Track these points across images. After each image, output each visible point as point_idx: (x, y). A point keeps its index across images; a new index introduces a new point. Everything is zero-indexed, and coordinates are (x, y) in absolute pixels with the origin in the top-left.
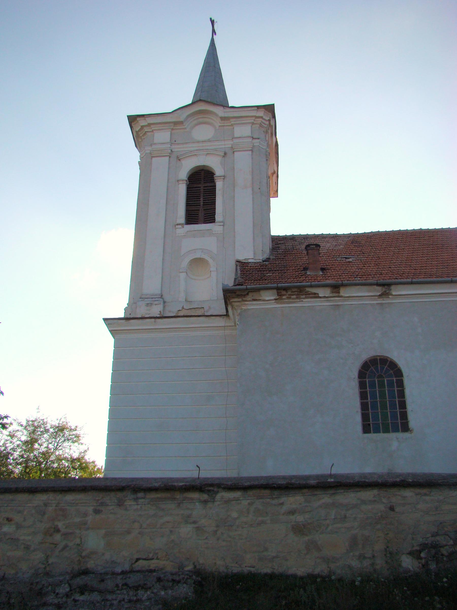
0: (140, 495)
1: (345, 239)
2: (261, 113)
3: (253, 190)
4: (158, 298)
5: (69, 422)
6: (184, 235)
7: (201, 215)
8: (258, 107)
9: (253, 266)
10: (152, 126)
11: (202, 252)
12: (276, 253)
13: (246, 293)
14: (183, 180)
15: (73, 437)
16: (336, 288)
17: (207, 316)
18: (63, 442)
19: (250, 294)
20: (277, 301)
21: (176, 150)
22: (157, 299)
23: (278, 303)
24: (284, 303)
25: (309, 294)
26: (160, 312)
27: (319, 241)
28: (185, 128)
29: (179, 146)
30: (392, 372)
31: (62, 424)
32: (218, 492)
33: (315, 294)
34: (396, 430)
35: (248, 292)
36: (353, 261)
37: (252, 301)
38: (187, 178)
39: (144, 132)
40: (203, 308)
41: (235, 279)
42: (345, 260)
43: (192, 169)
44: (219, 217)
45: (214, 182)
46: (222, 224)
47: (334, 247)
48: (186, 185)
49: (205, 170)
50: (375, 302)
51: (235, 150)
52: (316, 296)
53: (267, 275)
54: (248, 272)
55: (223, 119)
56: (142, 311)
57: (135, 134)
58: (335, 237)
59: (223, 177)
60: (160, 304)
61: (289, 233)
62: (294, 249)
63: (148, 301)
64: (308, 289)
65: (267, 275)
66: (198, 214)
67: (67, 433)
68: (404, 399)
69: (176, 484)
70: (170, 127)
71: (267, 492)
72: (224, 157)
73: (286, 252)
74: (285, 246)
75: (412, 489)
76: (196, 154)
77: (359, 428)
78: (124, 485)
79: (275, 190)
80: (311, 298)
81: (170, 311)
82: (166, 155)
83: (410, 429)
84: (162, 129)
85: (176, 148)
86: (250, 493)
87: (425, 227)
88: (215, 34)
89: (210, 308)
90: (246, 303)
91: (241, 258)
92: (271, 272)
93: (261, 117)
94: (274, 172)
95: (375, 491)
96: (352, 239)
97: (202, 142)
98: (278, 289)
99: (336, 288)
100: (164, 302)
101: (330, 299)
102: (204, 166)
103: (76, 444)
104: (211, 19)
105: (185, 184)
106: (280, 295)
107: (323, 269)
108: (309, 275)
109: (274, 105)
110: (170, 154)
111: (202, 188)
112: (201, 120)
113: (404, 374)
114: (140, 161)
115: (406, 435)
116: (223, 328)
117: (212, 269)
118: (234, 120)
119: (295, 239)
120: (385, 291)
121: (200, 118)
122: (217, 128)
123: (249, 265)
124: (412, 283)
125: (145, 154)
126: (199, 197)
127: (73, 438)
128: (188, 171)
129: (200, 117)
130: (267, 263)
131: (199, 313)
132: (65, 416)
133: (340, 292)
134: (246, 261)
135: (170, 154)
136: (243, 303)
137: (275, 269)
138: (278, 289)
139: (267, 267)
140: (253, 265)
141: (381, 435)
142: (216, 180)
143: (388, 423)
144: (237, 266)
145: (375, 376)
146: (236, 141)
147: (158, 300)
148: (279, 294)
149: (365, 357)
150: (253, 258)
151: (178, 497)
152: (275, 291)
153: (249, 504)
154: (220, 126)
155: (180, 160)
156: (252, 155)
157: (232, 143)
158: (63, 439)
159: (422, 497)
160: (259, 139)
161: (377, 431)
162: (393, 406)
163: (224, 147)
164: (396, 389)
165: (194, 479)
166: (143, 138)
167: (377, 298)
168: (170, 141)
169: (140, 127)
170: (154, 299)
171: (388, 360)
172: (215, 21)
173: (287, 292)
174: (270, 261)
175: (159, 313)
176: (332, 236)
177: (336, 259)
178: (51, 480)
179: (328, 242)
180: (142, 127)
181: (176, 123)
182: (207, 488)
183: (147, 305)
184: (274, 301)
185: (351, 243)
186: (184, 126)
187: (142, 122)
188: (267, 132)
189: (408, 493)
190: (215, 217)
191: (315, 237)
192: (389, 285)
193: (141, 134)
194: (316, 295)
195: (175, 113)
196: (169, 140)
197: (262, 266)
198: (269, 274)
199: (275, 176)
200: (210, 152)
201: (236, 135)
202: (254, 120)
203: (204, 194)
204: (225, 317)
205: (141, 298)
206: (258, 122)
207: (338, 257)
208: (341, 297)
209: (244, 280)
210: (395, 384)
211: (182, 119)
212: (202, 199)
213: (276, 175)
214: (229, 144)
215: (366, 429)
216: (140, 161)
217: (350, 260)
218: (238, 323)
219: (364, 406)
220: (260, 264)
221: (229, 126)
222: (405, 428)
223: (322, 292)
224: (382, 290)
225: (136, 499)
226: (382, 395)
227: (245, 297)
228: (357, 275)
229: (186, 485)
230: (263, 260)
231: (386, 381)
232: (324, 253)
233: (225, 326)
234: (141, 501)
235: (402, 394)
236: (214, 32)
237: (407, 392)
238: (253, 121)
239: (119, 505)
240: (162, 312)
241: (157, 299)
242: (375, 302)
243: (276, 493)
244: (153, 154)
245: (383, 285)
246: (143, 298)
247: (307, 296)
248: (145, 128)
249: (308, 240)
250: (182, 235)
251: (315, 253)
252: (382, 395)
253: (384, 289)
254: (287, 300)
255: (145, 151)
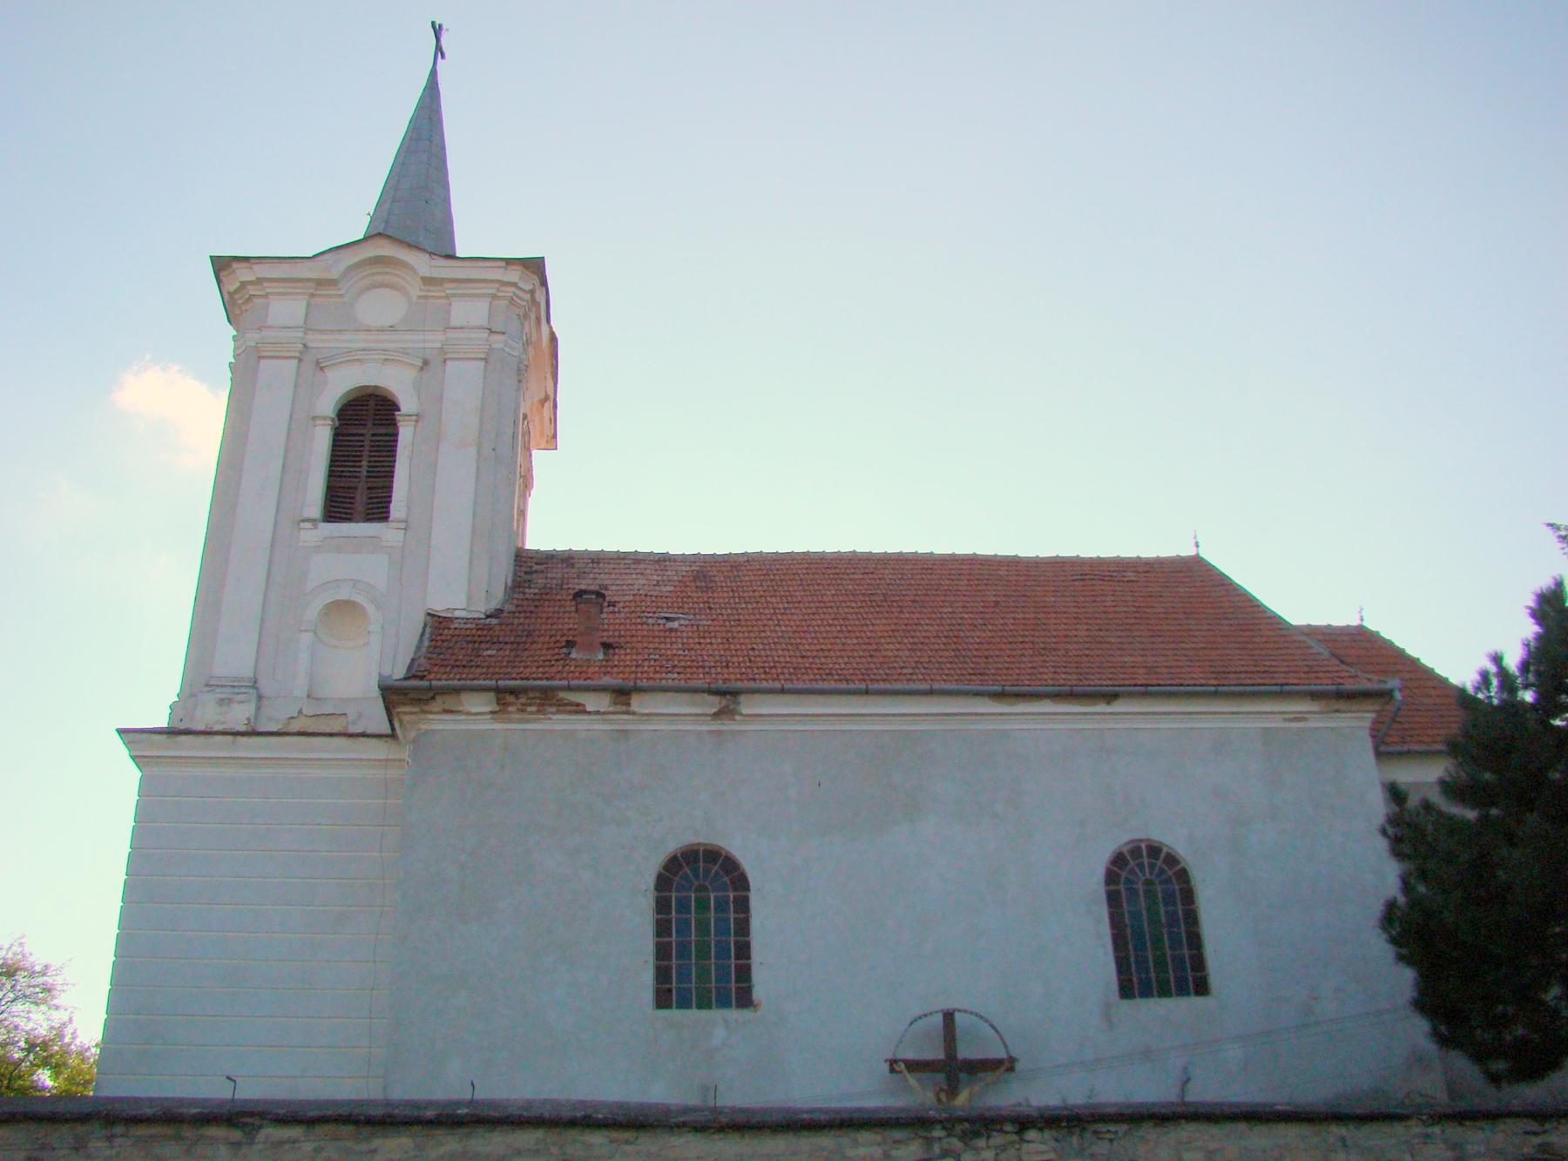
0: (119, 1129)
1: (684, 568)
2: (514, 275)
3: (479, 453)
4: (246, 686)
5: (31, 954)
6: (315, 547)
7: (361, 498)
8: (509, 262)
9: (461, 629)
10: (265, 285)
11: (354, 586)
12: (521, 596)
13: (431, 695)
14: (324, 418)
15: (37, 990)
16: (622, 694)
17: (351, 735)
18: (12, 1002)
19: (439, 699)
20: (495, 716)
21: (314, 345)
22: (243, 690)
23: (496, 720)
24: (510, 721)
25: (566, 705)
26: (248, 719)
27: (624, 571)
28: (341, 296)
29: (324, 337)
30: (726, 879)
31: (12, 959)
32: (261, 1127)
33: (578, 705)
34: (724, 1002)
35: (433, 694)
36: (680, 629)
37: (441, 713)
38: (335, 413)
39: (247, 296)
40: (345, 714)
41: (413, 660)
42: (664, 624)
43: (349, 392)
44: (397, 508)
45: (395, 425)
46: (402, 525)
47: (652, 588)
48: (331, 429)
49: (377, 396)
50: (704, 728)
51: (448, 356)
52: (579, 709)
53: (485, 653)
54: (445, 644)
55: (428, 281)
56: (208, 714)
57: (226, 296)
58: (662, 561)
59: (415, 418)
60: (250, 701)
61: (561, 545)
62: (562, 589)
63: (221, 693)
64: (562, 695)
65: (485, 653)
66: (353, 498)
67: (21, 978)
68: (747, 939)
69: (185, 1110)
70: (307, 291)
71: (349, 1129)
72: (422, 369)
73: (544, 596)
74: (547, 578)
75: (605, 1132)
76: (360, 357)
77: (648, 995)
78: (90, 1110)
79: (551, 434)
80: (570, 712)
81: (270, 719)
82: (293, 354)
83: (755, 1003)
84: (291, 294)
85: (315, 340)
86: (320, 1130)
87: (863, 547)
88: (443, 57)
89: (360, 715)
90: (431, 717)
91: (439, 605)
92: (496, 646)
93: (515, 285)
94: (547, 398)
95: (540, 1133)
96: (698, 568)
97: (378, 331)
98: (498, 691)
99: (622, 694)
100: (260, 697)
101: (606, 717)
102: (376, 387)
103: (43, 1007)
104: (433, 24)
105: (329, 427)
106: (504, 704)
107: (607, 646)
108: (575, 659)
109: (543, 258)
110: (301, 352)
111: (368, 438)
112: (379, 278)
113: (751, 888)
114: (233, 361)
115: (746, 1014)
116: (384, 763)
117: (372, 628)
118: (454, 285)
119: (574, 561)
120: (727, 706)
121: (378, 273)
122: (414, 299)
123: (453, 626)
124: (783, 691)
125: (244, 348)
126: (358, 464)
127: (38, 993)
128: (339, 395)
129: (374, 271)
130: (494, 621)
131: (336, 726)
132: (22, 941)
133: (632, 702)
134: (450, 615)
135: (301, 352)
136: (423, 716)
137: (507, 639)
138: (498, 691)
139: (491, 633)
140: (462, 626)
141: (693, 1014)
142: (399, 421)
143: (711, 989)
144: (425, 625)
145: (690, 888)
146: (453, 335)
147: (245, 693)
148: (503, 704)
149: (673, 845)
150: (464, 607)
151: (188, 1134)
152: (492, 695)
153: (315, 1150)
154: (420, 297)
155: (322, 369)
156: (485, 371)
157: (443, 338)
158: (11, 995)
159: (623, 1146)
160: (504, 333)
161: (684, 1004)
162: (723, 952)
163: (422, 345)
164: (732, 916)
165: (222, 1103)
166: (243, 308)
167: (709, 718)
168: (305, 323)
169: (238, 284)
170: (236, 690)
171: (721, 855)
172: (444, 27)
173: (517, 697)
174: (502, 616)
175: (246, 722)
176: (657, 558)
177: (644, 620)
178: (1523, 703)
179: (642, 574)
180: (244, 285)
181: (320, 283)
182: (242, 1120)
183: (221, 702)
184: (489, 717)
185: (692, 578)
186: (339, 289)
187: (244, 274)
188: (526, 316)
189: (597, 1139)
190: (389, 507)
191: (619, 558)
192: (735, 694)
193: (240, 298)
194: (581, 708)
195: (321, 258)
196: (301, 323)
197: (481, 629)
198: (489, 652)
199: (549, 405)
200: (391, 355)
201: (453, 323)
202: (498, 290)
203: (370, 451)
204: (389, 739)
205: (207, 685)
206: (508, 294)
207: (651, 615)
208: (634, 713)
209: (431, 664)
210: (732, 905)
211: (335, 274)
212: (364, 463)
213: (552, 403)
214: (434, 340)
215: (663, 999)
216: (233, 361)
217: (675, 625)
218: (410, 761)
219: (662, 952)
220: (477, 625)
221: (440, 297)
222: (745, 999)
223: (592, 702)
224: (720, 703)
225: (110, 1138)
226: (703, 928)
227: (427, 705)
228: (674, 667)
229: (202, 1113)
230: (488, 613)
231: (712, 898)
232: (625, 602)
233: (387, 760)
234: (118, 1141)
235: (743, 927)
236: (439, 51)
237: (755, 923)
238: (494, 291)
239: (77, 1149)
240: (252, 720)
241: (243, 690)
242: (704, 728)
243: (366, 1131)
244: (264, 351)
245: (721, 693)
246: (212, 685)
247: (561, 708)
248: (248, 287)
249: (601, 565)
250: (313, 544)
251: (592, 610)
252: (703, 928)
253: (724, 702)
254: (517, 716)
255: (245, 341)
